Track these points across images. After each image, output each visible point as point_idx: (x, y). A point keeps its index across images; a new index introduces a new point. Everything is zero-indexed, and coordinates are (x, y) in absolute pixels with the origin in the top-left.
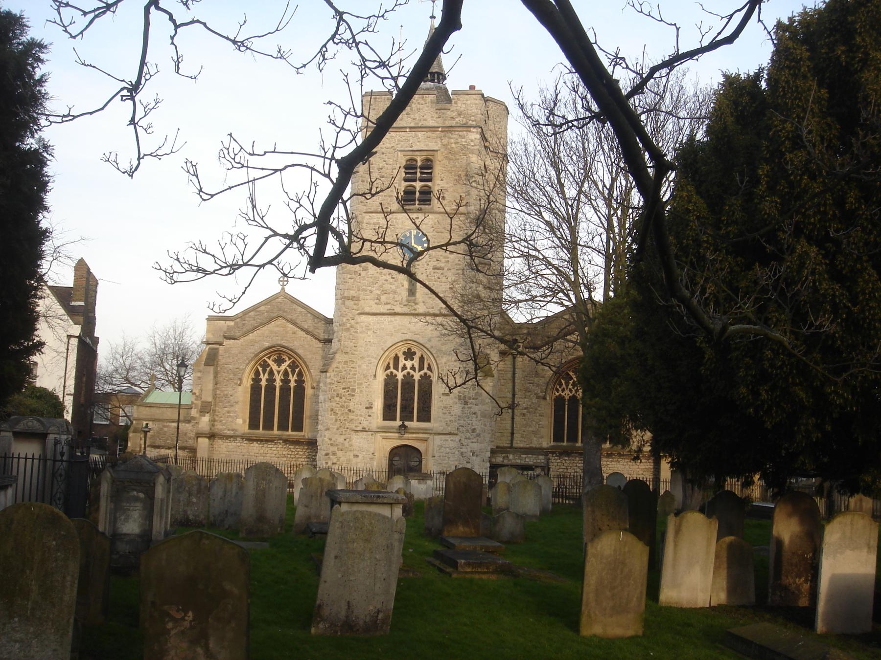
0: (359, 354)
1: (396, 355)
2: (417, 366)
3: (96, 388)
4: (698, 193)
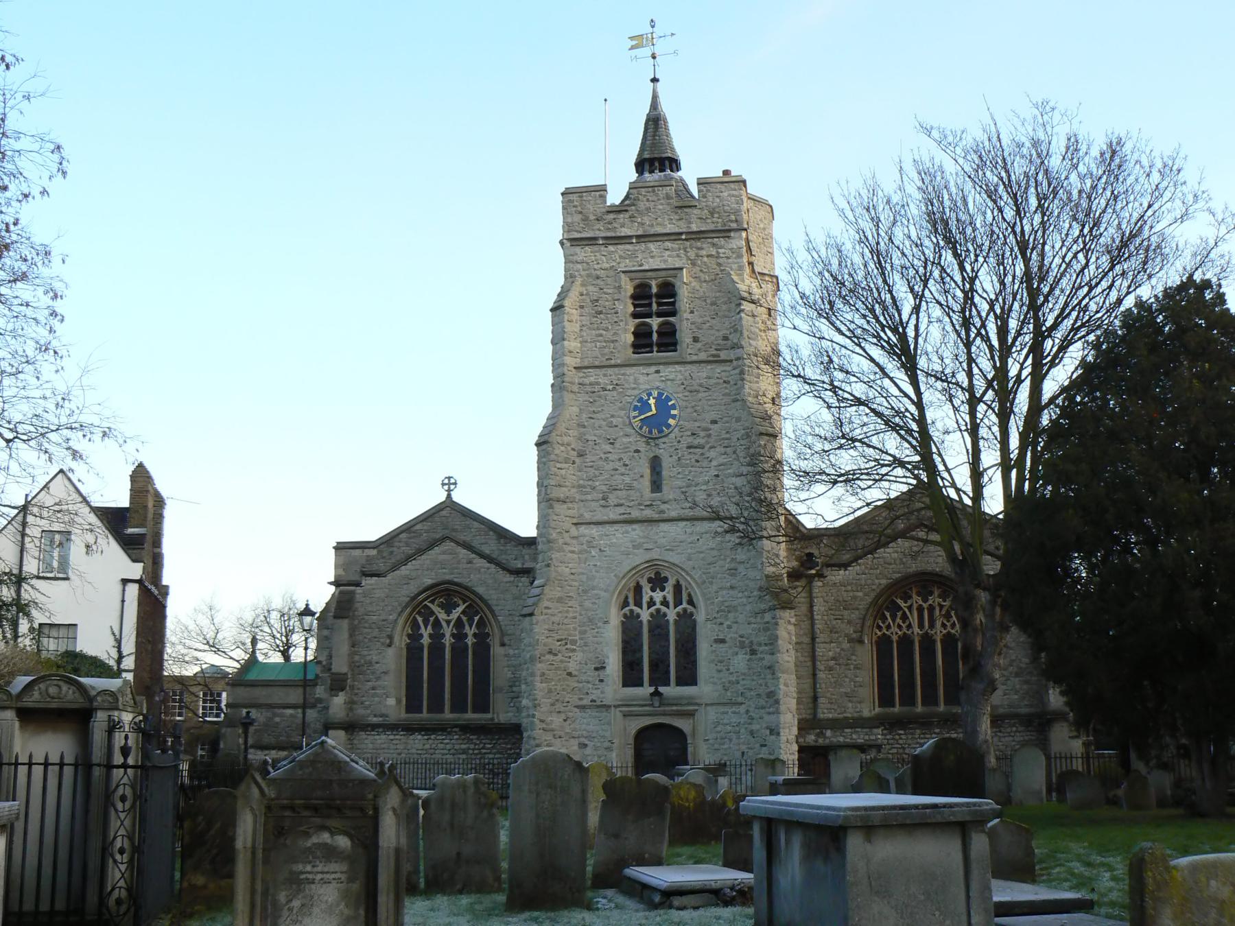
2: (670, 598)
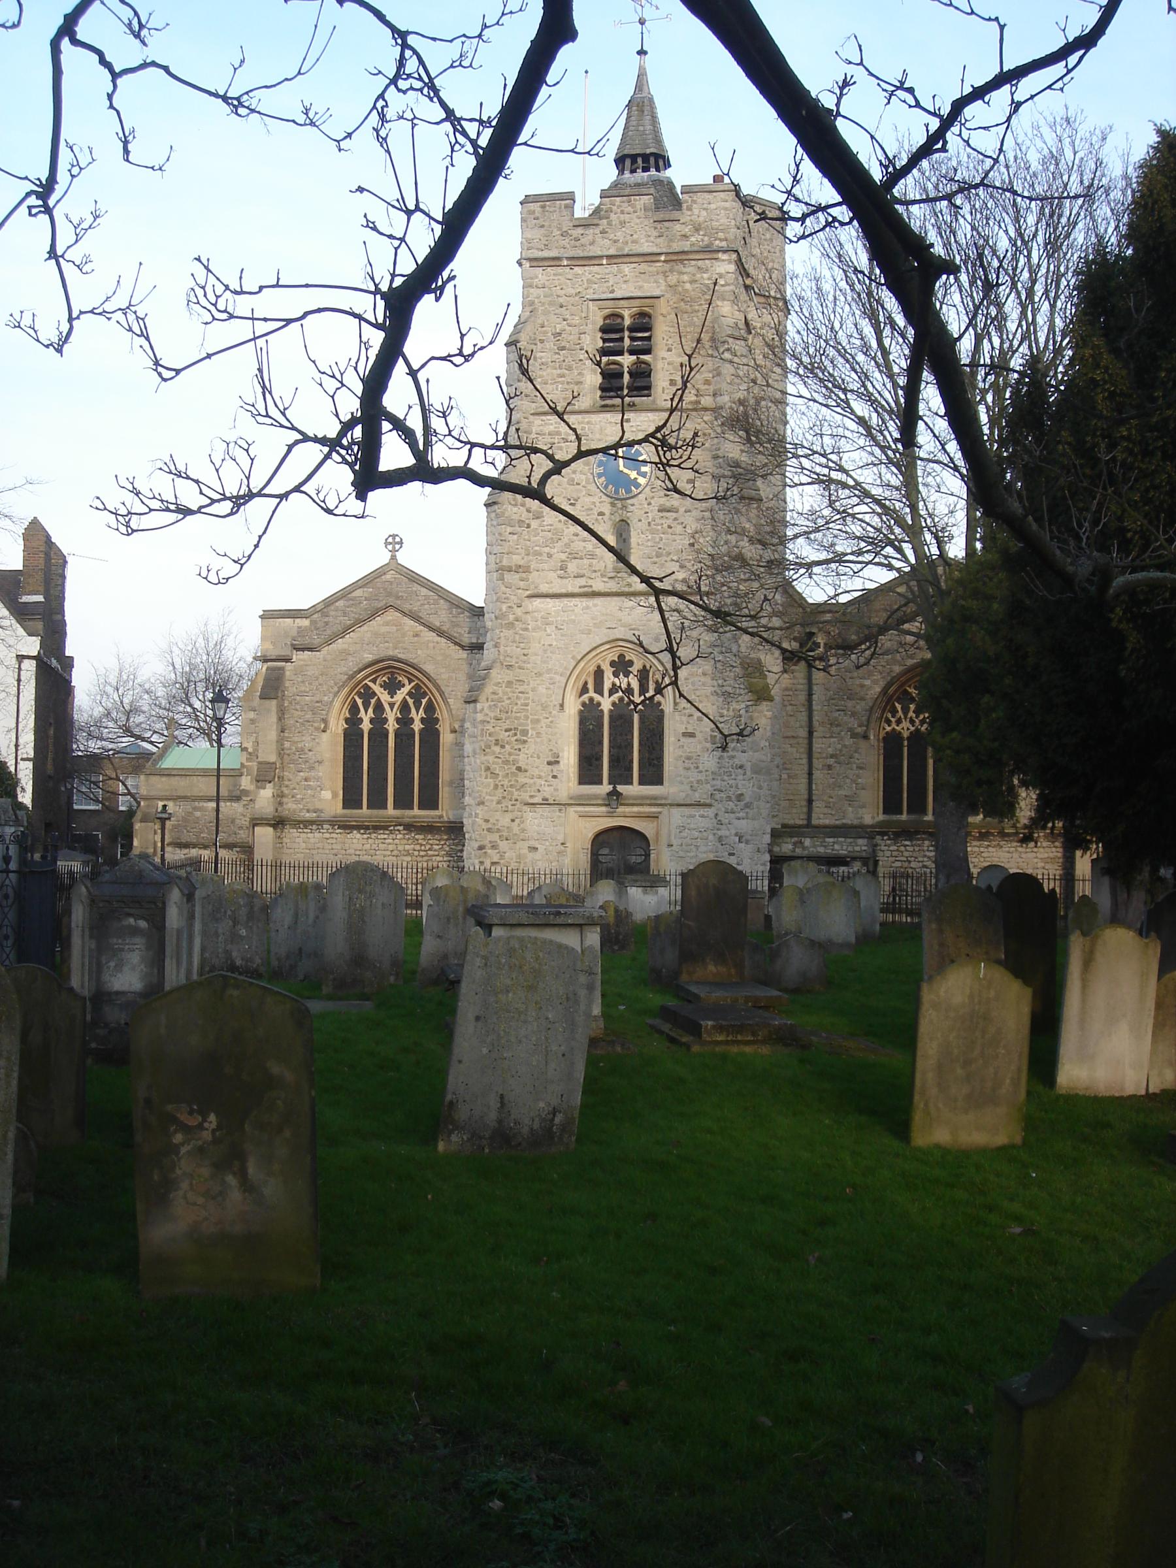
0: (533, 668)
1: (599, 667)
3: (75, 746)
4: (1115, 352)
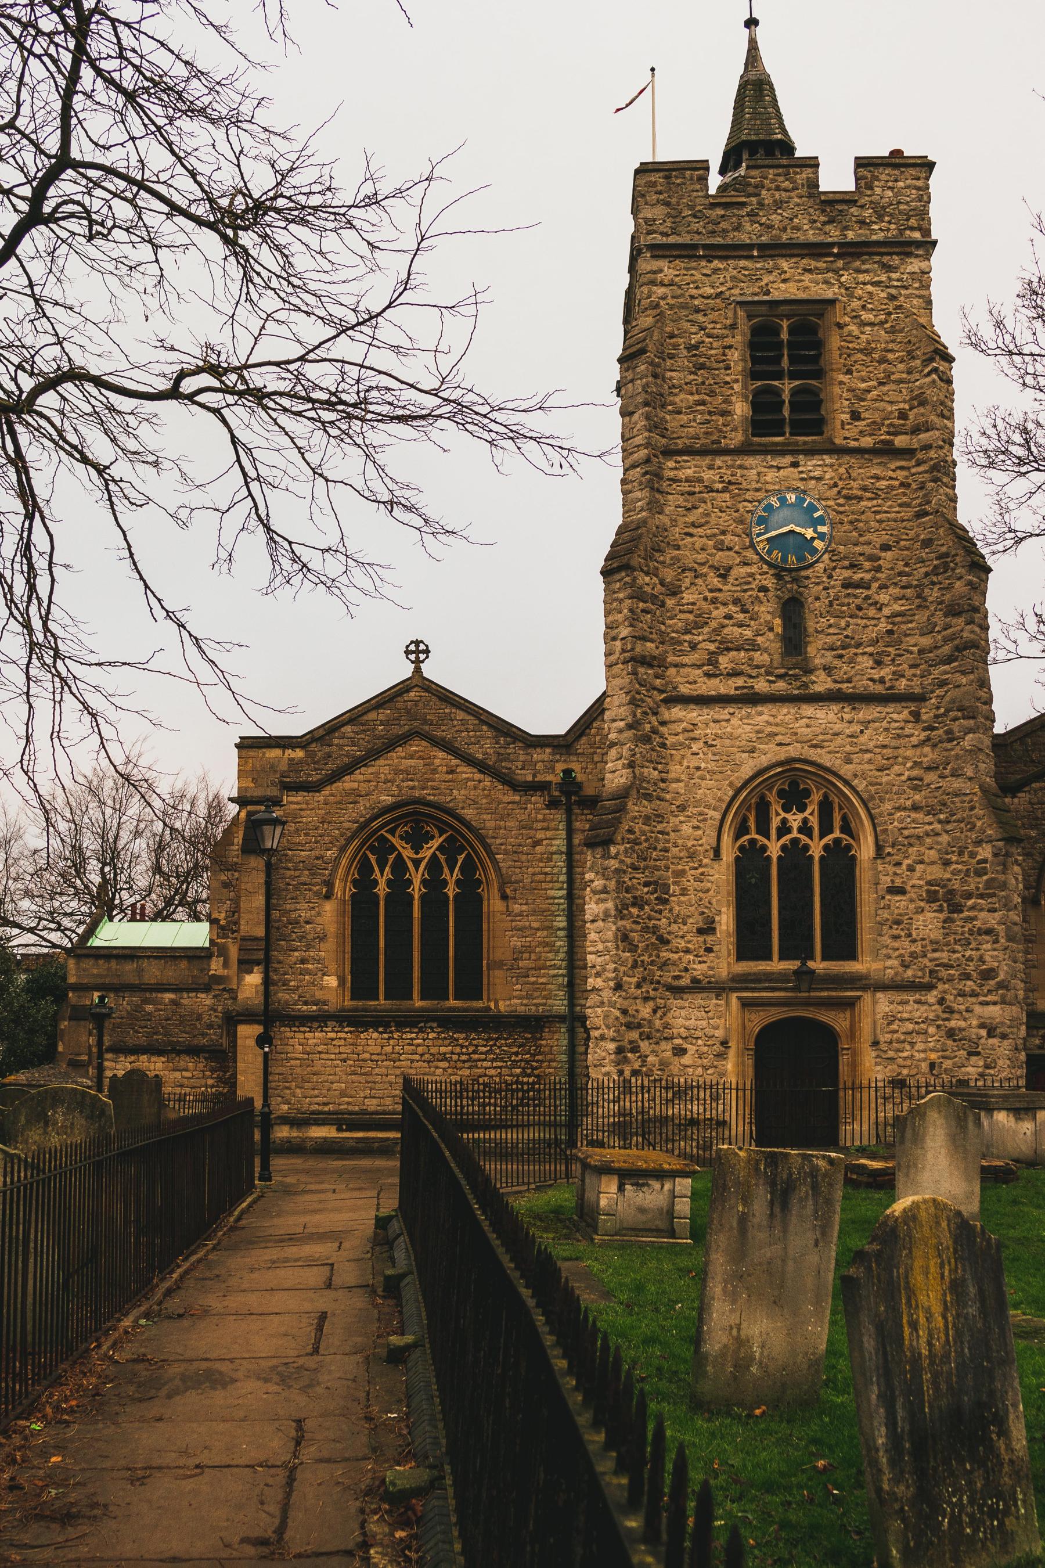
0: (674, 799)
2: (814, 822)
